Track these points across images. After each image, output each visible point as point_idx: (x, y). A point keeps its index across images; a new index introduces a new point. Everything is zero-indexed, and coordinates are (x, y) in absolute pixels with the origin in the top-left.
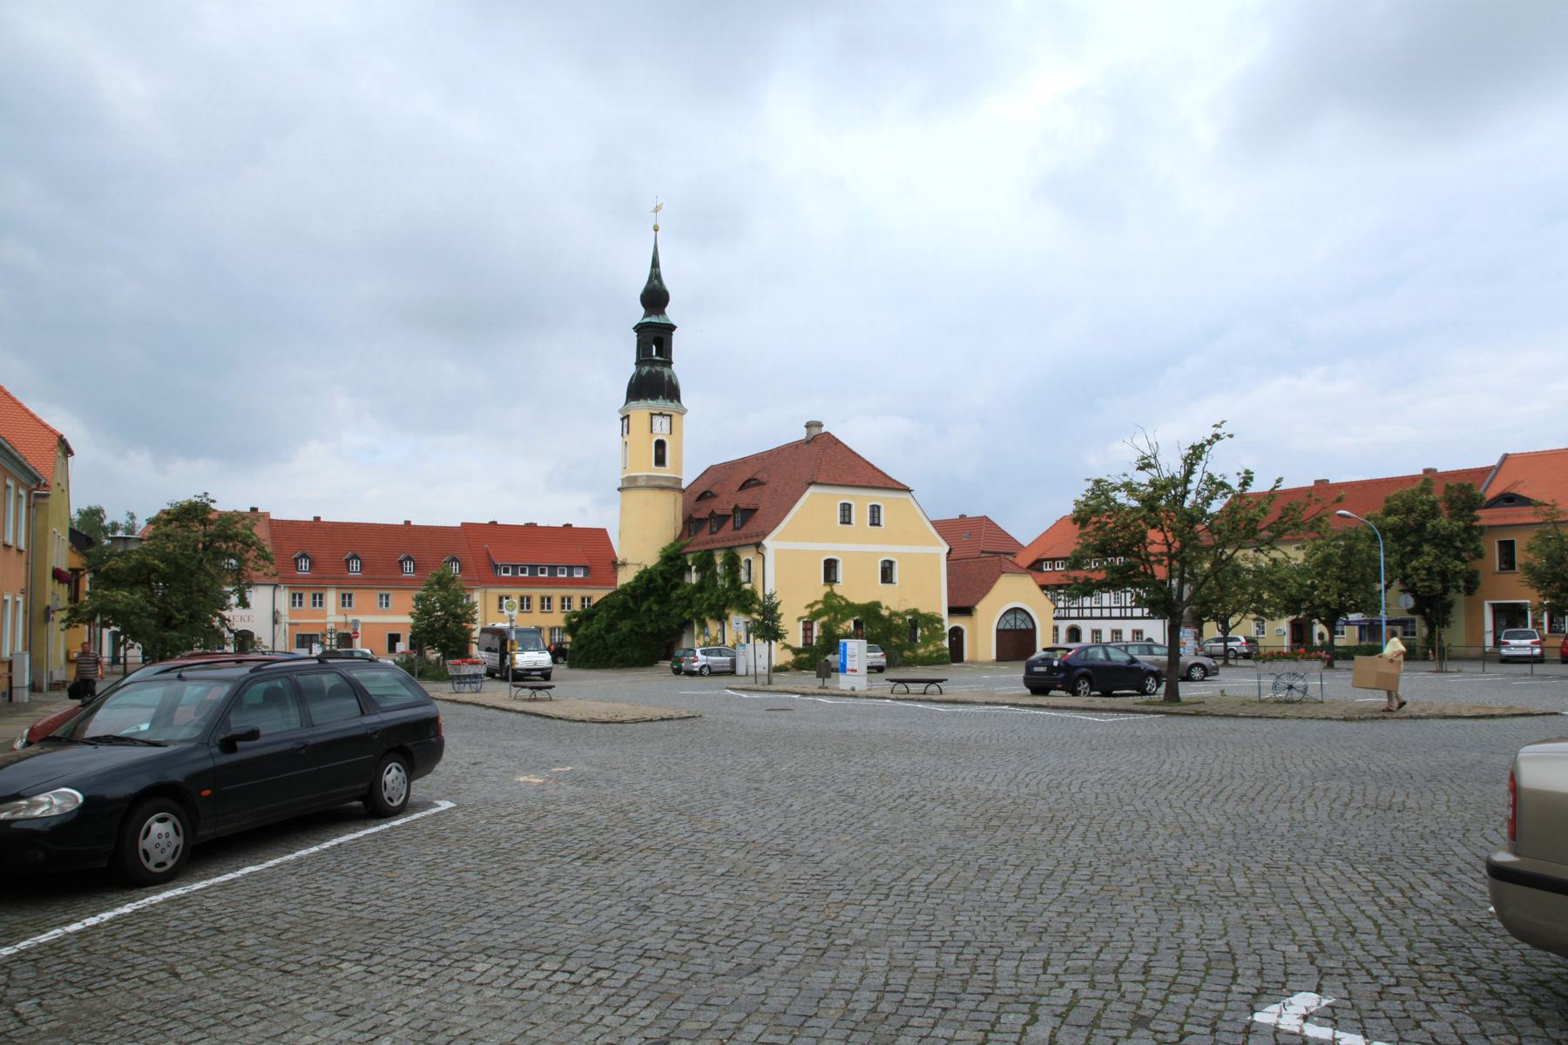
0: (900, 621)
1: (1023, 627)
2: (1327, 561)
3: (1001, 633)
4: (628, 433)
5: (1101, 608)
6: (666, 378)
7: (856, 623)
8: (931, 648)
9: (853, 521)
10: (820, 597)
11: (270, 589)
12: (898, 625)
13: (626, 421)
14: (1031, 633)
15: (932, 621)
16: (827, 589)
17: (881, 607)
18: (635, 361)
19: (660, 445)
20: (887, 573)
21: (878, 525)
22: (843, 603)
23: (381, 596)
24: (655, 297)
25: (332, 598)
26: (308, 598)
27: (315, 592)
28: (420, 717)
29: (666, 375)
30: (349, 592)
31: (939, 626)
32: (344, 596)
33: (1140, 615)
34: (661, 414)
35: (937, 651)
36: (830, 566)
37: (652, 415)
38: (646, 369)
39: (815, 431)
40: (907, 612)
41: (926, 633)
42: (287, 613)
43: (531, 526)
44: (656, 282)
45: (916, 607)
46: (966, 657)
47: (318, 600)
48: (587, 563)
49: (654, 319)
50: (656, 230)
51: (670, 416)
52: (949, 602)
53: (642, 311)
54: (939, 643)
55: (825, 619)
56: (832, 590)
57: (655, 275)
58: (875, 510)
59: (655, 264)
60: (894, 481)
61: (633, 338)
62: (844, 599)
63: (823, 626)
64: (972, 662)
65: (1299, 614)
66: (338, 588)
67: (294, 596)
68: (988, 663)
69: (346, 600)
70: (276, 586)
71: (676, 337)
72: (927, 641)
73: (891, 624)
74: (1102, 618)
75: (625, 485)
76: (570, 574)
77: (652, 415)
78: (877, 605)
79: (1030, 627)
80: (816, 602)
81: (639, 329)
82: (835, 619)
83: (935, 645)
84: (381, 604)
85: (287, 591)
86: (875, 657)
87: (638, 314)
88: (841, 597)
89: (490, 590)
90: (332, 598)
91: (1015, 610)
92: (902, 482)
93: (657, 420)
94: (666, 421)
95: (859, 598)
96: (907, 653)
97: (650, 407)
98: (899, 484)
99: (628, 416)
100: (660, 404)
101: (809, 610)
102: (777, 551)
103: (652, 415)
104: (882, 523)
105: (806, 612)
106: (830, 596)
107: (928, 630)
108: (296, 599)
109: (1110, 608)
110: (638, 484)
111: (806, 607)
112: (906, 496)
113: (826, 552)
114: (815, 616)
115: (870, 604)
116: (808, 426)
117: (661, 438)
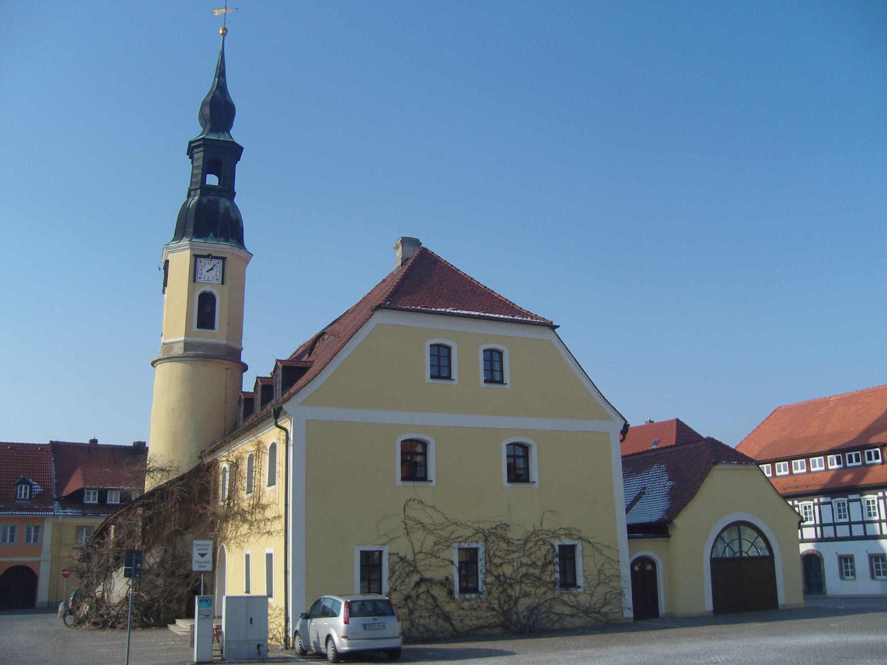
1: (752, 553)
5: (850, 523)
6: (222, 211)
9: (454, 375)
21: (501, 382)
29: (221, 206)
51: (224, 259)
52: (459, 559)
57: (221, 87)
58: (493, 359)
59: (221, 73)
74: (851, 538)
98: (527, 314)
104: (507, 378)
109: (834, 525)
112: (547, 334)
117: (207, 289)
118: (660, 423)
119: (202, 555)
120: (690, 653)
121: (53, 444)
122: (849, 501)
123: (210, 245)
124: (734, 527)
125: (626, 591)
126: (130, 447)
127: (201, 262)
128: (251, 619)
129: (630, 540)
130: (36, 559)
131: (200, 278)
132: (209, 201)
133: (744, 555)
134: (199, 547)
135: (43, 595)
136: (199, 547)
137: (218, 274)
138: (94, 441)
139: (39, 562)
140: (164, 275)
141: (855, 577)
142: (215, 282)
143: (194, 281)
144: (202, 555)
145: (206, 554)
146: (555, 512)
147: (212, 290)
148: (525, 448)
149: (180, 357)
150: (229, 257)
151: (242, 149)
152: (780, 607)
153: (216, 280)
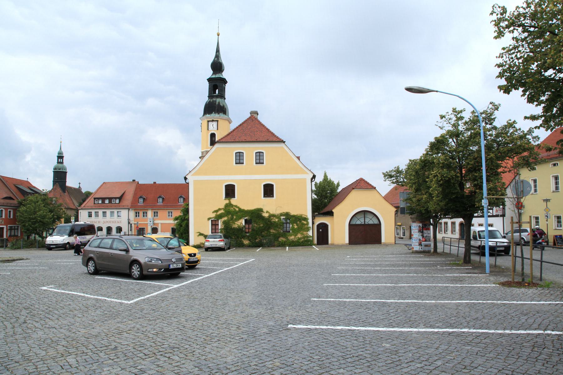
0: (277, 220)
1: (371, 222)
2: (426, 160)
3: (352, 227)
6: (217, 103)
7: (246, 221)
8: (299, 236)
10: (222, 206)
11: (127, 211)
12: (275, 222)
14: (378, 227)
15: (299, 219)
16: (227, 201)
17: (262, 211)
18: (208, 95)
20: (269, 190)
22: (237, 209)
23: (169, 213)
24: (217, 66)
25: (150, 213)
26: (141, 214)
27: (155, 211)
30: (145, 211)
31: (305, 222)
32: (155, 213)
34: (213, 121)
35: (304, 238)
36: (230, 191)
37: (208, 121)
40: (282, 215)
41: (296, 227)
42: (133, 220)
45: (288, 211)
46: (330, 242)
47: (145, 214)
49: (218, 76)
50: (218, 35)
51: (217, 121)
53: (212, 72)
54: (305, 233)
55: (226, 218)
56: (230, 202)
57: (217, 56)
59: (218, 51)
60: (277, 137)
61: (207, 85)
62: (238, 207)
63: (224, 222)
64: (332, 245)
66: (152, 210)
67: (136, 213)
69: (156, 214)
70: (129, 209)
72: (295, 232)
73: (270, 221)
78: (260, 210)
79: (376, 222)
80: (220, 209)
81: (210, 80)
82: (232, 219)
83: (302, 234)
84: (169, 215)
85: (133, 211)
86: (214, 241)
87: (209, 73)
88: (236, 206)
90: (150, 213)
91: (365, 213)
92: (281, 138)
93: (210, 123)
94: (215, 124)
96: (282, 239)
97: (207, 118)
101: (215, 214)
102: (195, 182)
103: (208, 121)
105: (213, 215)
106: (229, 205)
107: (297, 225)
108: (137, 215)
111: (213, 212)
112: (282, 145)
113: (225, 181)
114: (220, 217)
117: (213, 132)
118: (160, 184)
119: (150, 222)
123: (214, 116)
124: (362, 213)
126: (75, 189)
132: (213, 101)
133: (366, 223)
138: (155, 183)
141: (91, 274)
143: (208, 130)
144: (150, 222)
146: (281, 207)
148: (272, 186)
150: (219, 120)
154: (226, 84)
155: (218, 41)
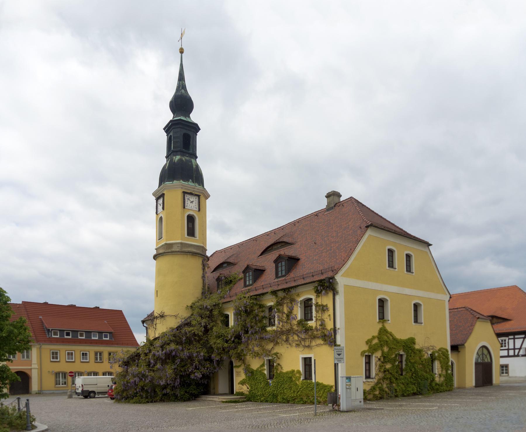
4: (163, 208)
6: (194, 167)
10: (376, 334)
13: (161, 201)
18: (165, 154)
19: (191, 219)
28: (195, 221)
33: (506, 354)
34: (191, 194)
38: (177, 158)
39: (336, 200)
43: (72, 307)
44: (183, 91)
48: (112, 331)
56: (383, 326)
65: (181, 160)
68: (470, 389)
71: (200, 138)
74: (508, 356)
75: (161, 251)
76: (101, 337)
77: (184, 193)
80: (374, 337)
89: (44, 347)
94: (195, 199)
95: (401, 335)
99: (163, 195)
100: (190, 185)
105: (366, 348)
106: (383, 331)
110: (173, 250)
112: (421, 248)
114: (373, 349)
115: (409, 339)
116: (328, 196)
117: (191, 213)
120: (361, 411)
121: (24, 303)
122: (509, 339)
125: (18, 397)
127: (187, 196)
128: (357, 388)
129: (452, 353)
130: (30, 367)
131: (187, 206)
132: (185, 159)
134: (337, 350)
135: (35, 386)
136: (337, 350)
137: (196, 204)
139: (31, 369)
140: (156, 203)
142: (195, 209)
145: (341, 354)
147: (194, 214)
149: (180, 252)
151: (200, 129)
152: (494, 385)
153: (195, 208)
154: (198, 132)
155: (181, 65)
